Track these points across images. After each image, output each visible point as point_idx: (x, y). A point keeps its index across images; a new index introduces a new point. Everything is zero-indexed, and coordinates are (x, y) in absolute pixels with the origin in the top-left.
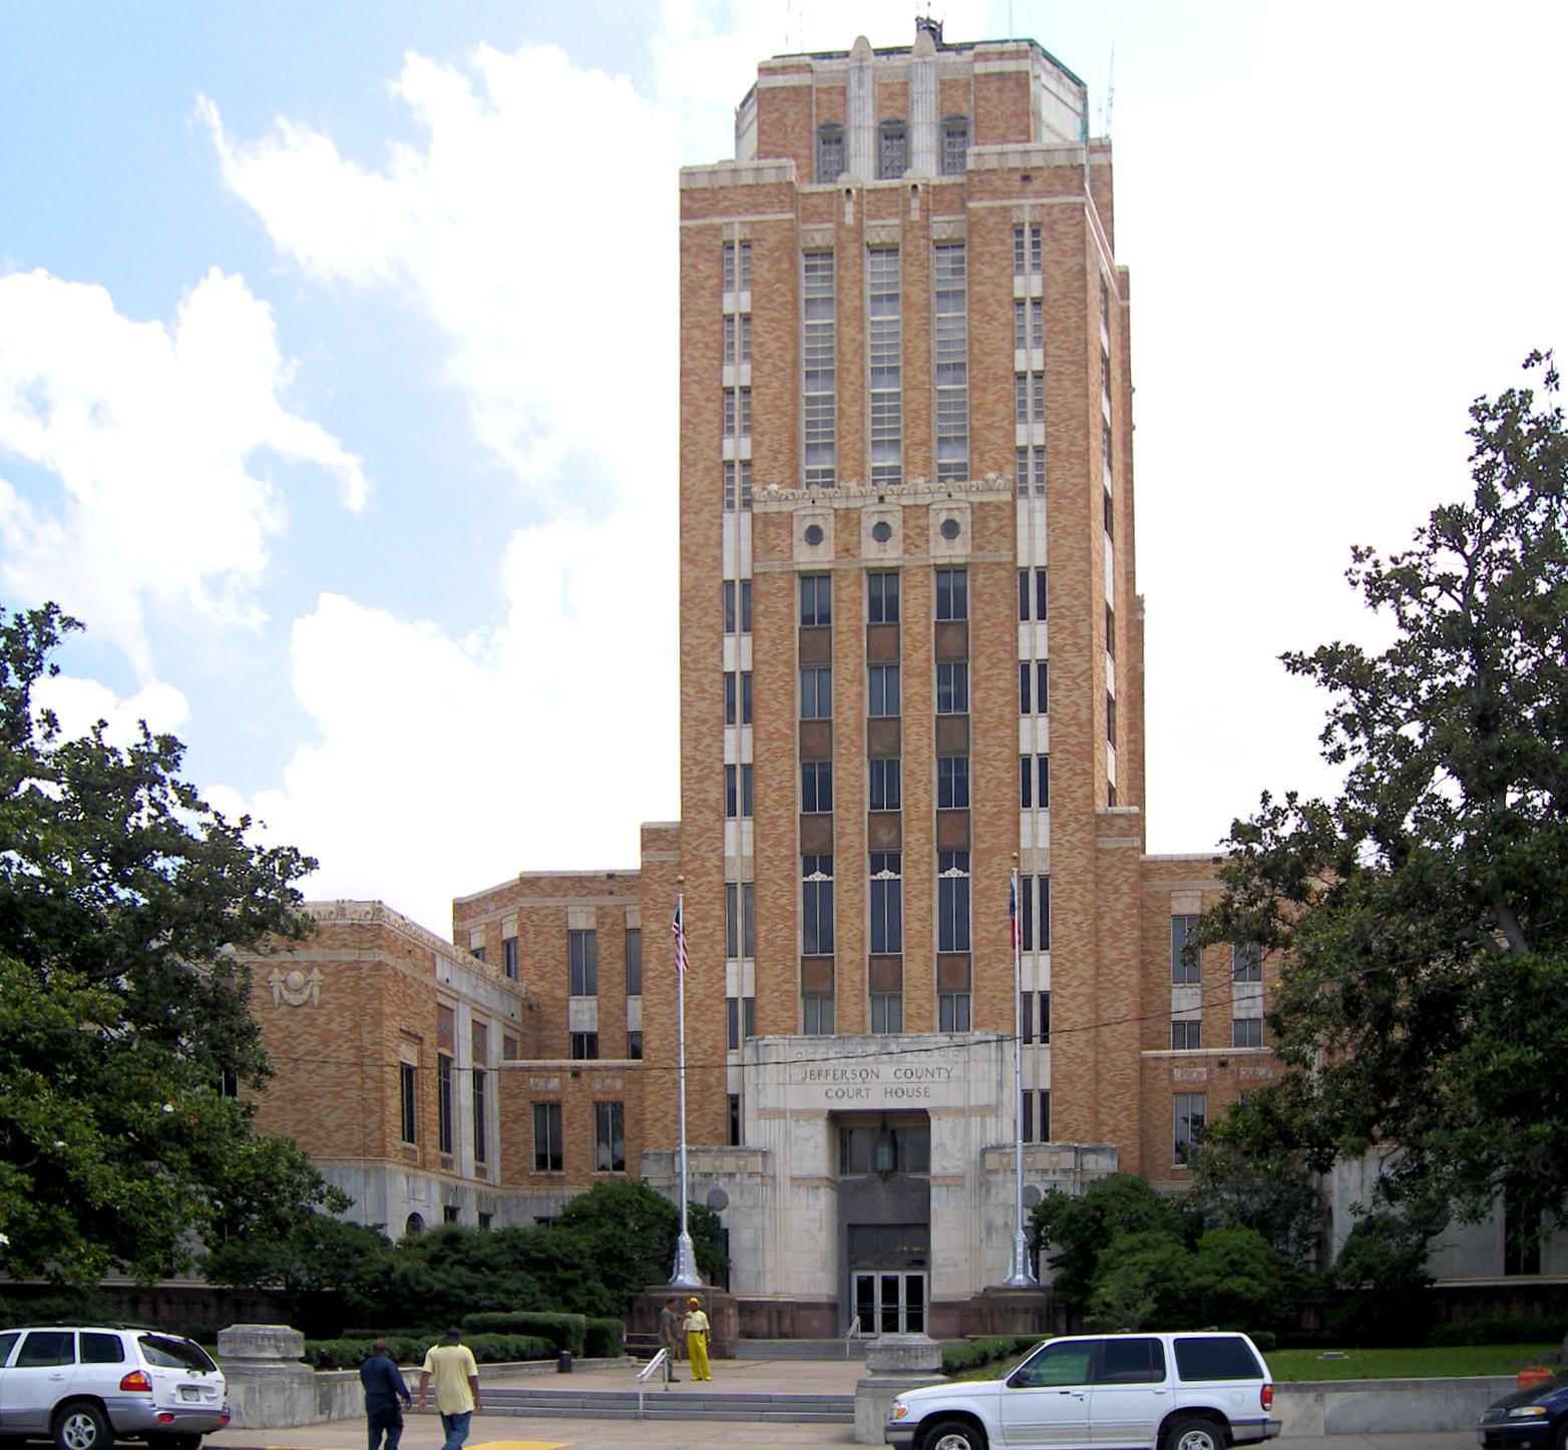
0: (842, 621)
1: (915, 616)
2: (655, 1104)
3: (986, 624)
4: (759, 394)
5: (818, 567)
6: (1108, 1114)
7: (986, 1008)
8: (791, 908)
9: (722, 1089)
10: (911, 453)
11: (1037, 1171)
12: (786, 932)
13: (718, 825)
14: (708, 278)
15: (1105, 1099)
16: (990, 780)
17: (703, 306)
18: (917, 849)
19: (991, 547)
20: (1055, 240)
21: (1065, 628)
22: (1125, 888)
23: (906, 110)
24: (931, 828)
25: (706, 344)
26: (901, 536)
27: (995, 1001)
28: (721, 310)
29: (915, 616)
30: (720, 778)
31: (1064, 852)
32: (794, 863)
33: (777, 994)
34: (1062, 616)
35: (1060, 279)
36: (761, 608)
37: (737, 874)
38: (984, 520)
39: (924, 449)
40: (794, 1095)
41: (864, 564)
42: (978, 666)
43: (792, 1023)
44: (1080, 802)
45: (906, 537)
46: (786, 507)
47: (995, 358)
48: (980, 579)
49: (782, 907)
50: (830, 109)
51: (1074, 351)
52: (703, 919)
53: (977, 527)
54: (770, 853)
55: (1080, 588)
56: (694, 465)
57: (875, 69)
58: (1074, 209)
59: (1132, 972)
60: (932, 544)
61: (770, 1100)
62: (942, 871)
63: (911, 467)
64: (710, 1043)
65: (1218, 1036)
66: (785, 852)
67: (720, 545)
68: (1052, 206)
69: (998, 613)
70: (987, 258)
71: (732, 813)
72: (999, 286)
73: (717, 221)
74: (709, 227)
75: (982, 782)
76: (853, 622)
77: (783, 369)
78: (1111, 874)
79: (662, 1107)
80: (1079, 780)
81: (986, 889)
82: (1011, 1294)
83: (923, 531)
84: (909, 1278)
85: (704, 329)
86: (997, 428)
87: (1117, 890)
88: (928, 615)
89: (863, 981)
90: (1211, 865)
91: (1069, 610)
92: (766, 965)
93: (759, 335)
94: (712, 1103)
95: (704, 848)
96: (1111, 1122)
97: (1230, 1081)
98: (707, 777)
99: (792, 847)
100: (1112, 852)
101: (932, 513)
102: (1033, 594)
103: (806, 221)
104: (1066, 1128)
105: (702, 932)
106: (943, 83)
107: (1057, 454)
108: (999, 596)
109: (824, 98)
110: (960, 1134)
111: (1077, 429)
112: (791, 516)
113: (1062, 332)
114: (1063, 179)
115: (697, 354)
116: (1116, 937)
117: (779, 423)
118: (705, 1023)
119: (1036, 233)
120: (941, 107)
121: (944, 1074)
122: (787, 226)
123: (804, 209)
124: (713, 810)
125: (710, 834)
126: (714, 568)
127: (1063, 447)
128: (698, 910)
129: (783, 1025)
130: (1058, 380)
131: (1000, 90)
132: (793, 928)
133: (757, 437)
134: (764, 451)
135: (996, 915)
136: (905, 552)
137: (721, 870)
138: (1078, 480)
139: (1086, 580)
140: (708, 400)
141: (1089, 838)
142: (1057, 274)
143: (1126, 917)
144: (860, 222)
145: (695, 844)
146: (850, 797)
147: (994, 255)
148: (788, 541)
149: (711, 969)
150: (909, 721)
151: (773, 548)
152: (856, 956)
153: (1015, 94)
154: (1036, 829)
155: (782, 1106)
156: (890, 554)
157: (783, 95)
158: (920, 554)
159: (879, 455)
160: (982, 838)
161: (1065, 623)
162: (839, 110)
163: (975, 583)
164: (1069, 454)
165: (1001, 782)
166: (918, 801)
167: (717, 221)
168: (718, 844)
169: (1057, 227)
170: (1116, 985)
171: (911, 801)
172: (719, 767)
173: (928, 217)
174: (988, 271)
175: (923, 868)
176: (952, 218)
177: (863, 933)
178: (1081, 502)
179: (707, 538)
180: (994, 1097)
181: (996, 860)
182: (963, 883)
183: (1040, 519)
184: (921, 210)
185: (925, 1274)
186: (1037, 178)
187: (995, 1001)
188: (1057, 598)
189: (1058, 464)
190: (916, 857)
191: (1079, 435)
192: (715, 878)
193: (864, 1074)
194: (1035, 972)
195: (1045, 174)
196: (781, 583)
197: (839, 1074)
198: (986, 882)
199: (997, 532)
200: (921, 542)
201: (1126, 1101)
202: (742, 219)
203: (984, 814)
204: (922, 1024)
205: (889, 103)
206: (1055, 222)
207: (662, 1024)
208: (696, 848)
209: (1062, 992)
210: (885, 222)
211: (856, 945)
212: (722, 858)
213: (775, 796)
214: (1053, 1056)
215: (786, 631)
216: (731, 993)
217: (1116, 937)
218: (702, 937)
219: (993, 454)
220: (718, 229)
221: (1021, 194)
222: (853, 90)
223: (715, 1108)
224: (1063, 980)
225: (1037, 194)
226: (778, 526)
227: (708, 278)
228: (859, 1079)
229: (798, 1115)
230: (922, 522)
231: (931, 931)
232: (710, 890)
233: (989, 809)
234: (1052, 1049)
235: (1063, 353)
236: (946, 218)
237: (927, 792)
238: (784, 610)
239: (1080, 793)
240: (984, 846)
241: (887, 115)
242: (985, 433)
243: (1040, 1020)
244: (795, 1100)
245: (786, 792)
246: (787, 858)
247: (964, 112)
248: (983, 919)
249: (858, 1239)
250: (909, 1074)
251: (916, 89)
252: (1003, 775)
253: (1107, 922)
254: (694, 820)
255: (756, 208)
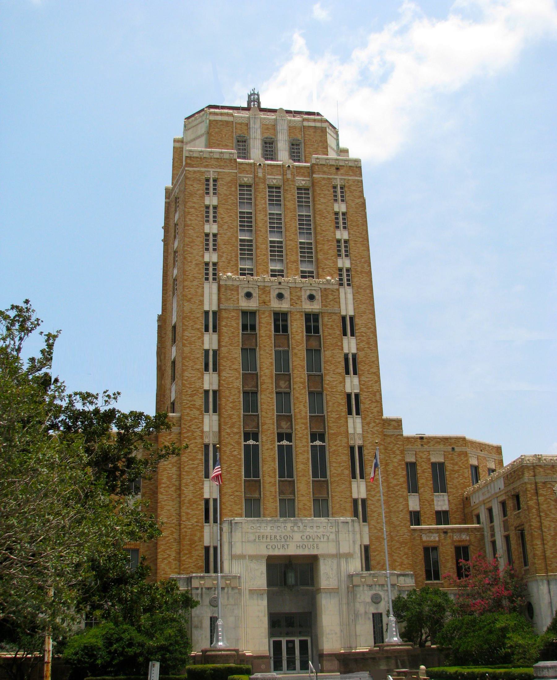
0: (262, 332)
1: (296, 332)
2: (164, 551)
3: (329, 337)
4: (221, 237)
5: (250, 308)
6: (398, 556)
7: (337, 506)
8: (239, 456)
9: (201, 543)
10: (290, 265)
11: (379, 585)
12: (236, 468)
13: (200, 417)
14: (198, 190)
15: (396, 549)
16: (334, 405)
17: (195, 200)
18: (301, 432)
19: (331, 306)
20: (351, 192)
21: (364, 341)
22: (398, 452)
23: (276, 135)
24: (307, 423)
25: (197, 215)
26: (289, 299)
27: (341, 502)
28: (204, 203)
29: (296, 332)
30: (201, 395)
31: (369, 435)
32: (240, 436)
33: (232, 497)
34: (363, 336)
35: (353, 206)
36: (224, 323)
37: (210, 440)
38: (327, 295)
39: (295, 264)
40: (249, 547)
41: (272, 309)
42: (326, 354)
43: (240, 511)
44: (376, 414)
45: (291, 299)
46: (236, 283)
47: (327, 233)
48: (326, 319)
49: (235, 456)
50: (241, 131)
51: (361, 233)
52: (193, 460)
53: (324, 298)
54: (228, 431)
55: (370, 325)
56: (191, 262)
57: (261, 119)
58: (358, 182)
59: (404, 490)
60: (303, 303)
61: (238, 550)
62: (312, 442)
63: (289, 271)
64: (195, 520)
65: (428, 518)
66: (236, 430)
67: (203, 296)
68: (349, 180)
69: (335, 333)
70: (322, 195)
71: (207, 411)
72: (328, 206)
73: (203, 169)
74: (199, 171)
75: (330, 403)
76: (268, 332)
77: (232, 228)
78: (391, 446)
79: (168, 552)
80: (374, 405)
81: (335, 451)
82: (223, 653)
83: (299, 298)
84: (300, 641)
85: (196, 209)
86: (330, 259)
87: (394, 453)
88: (302, 332)
89: (276, 492)
90: (419, 440)
91: (365, 333)
92: (226, 483)
93: (222, 214)
94: (196, 550)
95: (193, 427)
96: (399, 560)
97: (449, 541)
98: (195, 394)
99: (239, 428)
100: (391, 436)
101: (303, 291)
102: (348, 326)
103: (241, 173)
104: (378, 563)
105: (192, 466)
106: (289, 127)
107: (356, 271)
108: (335, 326)
109: (239, 126)
110: (335, 567)
111: (365, 262)
112: (238, 287)
113: (355, 226)
114: (353, 171)
115: (193, 218)
116: (395, 474)
117: (231, 249)
118: (193, 510)
119: (341, 188)
120: (289, 136)
121: (326, 538)
122: (234, 175)
123: (239, 168)
124: (198, 409)
125: (196, 421)
126: (200, 305)
127: (359, 269)
128: (190, 456)
129: (235, 512)
130: (355, 244)
131: (315, 132)
132: (240, 466)
133: (221, 254)
134: (223, 259)
135: (340, 463)
136: (291, 305)
137: (202, 437)
138: (366, 283)
139: (373, 322)
140: (198, 237)
141: (381, 430)
142: (353, 205)
143: (400, 465)
144: (264, 176)
145: (189, 424)
146: (268, 407)
147: (325, 195)
148: (237, 297)
149: (196, 484)
150: (295, 376)
151: (230, 299)
152: (272, 480)
153: (320, 134)
154: (355, 425)
155: (244, 553)
156: (285, 306)
157: (221, 123)
158: (298, 307)
159: (274, 264)
160: (332, 428)
161: (364, 339)
162: (245, 132)
163: (324, 321)
164: (361, 272)
165: (339, 404)
166: (301, 411)
167: (203, 169)
168: (200, 425)
169: (351, 187)
170: (397, 496)
171: (297, 411)
172: (201, 391)
173: (294, 177)
174: (322, 200)
175: (304, 440)
176: (304, 179)
177: (275, 469)
178: (368, 291)
179: (196, 292)
180: (352, 548)
181: (339, 438)
182: (322, 448)
183: (350, 296)
184: (291, 175)
185: (309, 639)
186: (342, 169)
187: (341, 502)
188: (360, 328)
189: (356, 275)
190: (301, 435)
191: (366, 265)
192: (199, 441)
193: (286, 538)
194: (359, 489)
195: (345, 168)
196: (233, 314)
197: (273, 537)
198: (334, 448)
199: (333, 300)
200: (298, 302)
201: (406, 550)
202: (214, 170)
203: (332, 418)
204: (307, 513)
205: (266, 131)
206: (350, 185)
207: (169, 510)
208: (189, 427)
209: (372, 499)
210: (276, 177)
211: (272, 475)
212: (202, 432)
213: (231, 405)
214: (370, 529)
215: (236, 334)
216: (206, 496)
217: (395, 474)
218: (193, 468)
219: (328, 269)
220: (203, 173)
221: (336, 174)
222: (252, 125)
223: (197, 553)
224: (373, 493)
225: (342, 174)
226: (232, 290)
227: (198, 190)
228: (283, 540)
229: (252, 557)
230: (299, 294)
231: (309, 469)
232: (196, 446)
233: (334, 415)
234: (369, 525)
235: (357, 233)
236: (302, 179)
237: (305, 407)
238: (233, 326)
239: (375, 410)
240: (333, 432)
241: (266, 135)
242: (324, 260)
243: (360, 510)
244: (251, 550)
245: (237, 404)
246: (237, 433)
247: (299, 137)
248: (334, 465)
249: (278, 623)
250: (308, 537)
251: (279, 128)
252: (340, 401)
253: (391, 467)
254: (188, 414)
255: (220, 167)
